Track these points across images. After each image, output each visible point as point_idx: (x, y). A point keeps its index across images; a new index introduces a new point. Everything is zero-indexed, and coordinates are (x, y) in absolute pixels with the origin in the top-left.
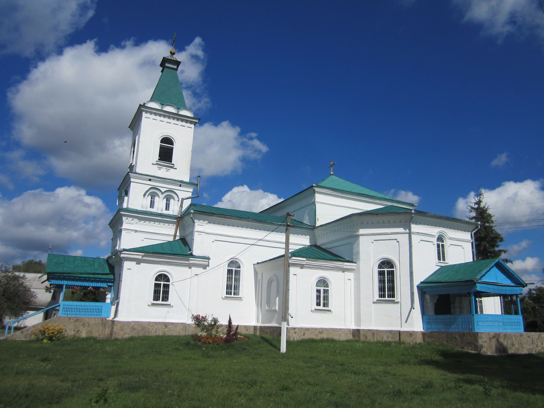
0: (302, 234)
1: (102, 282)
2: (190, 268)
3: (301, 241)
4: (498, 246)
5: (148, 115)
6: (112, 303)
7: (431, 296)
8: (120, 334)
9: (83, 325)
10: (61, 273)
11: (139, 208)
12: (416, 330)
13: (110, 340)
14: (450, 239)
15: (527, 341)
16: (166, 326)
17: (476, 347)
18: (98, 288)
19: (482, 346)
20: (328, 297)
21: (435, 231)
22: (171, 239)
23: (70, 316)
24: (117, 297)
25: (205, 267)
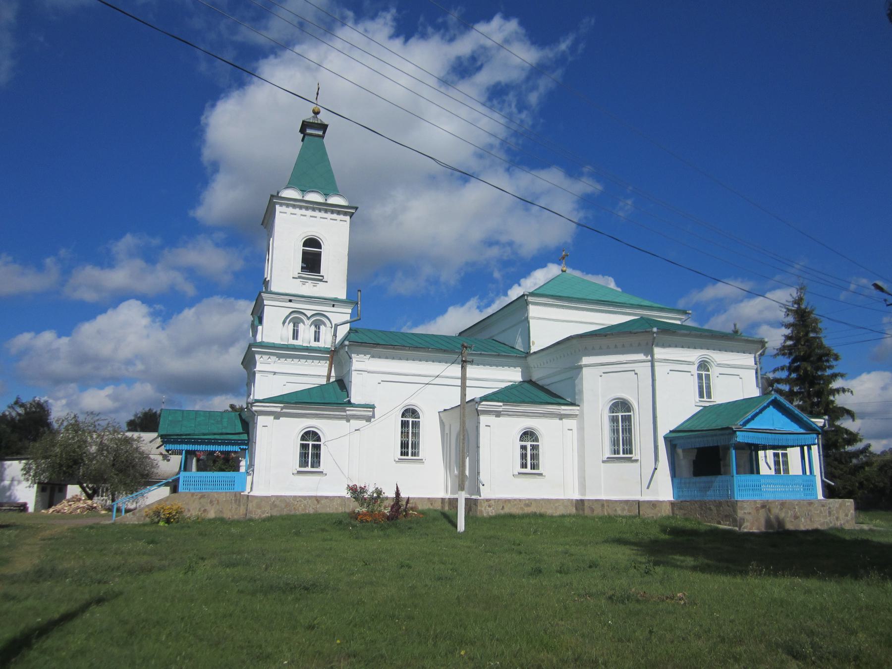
0: (503, 365)
1: (233, 444)
2: (348, 421)
3: (513, 375)
4: (830, 367)
5: (284, 209)
6: (247, 473)
7: (684, 451)
8: (258, 514)
9: (211, 502)
10: (178, 435)
11: (278, 341)
12: (661, 499)
13: (247, 522)
14: (719, 365)
15: (821, 512)
16: (318, 501)
17: (735, 522)
18: (229, 453)
19: (743, 520)
20: (537, 455)
21: (694, 355)
24: (251, 465)
25: (368, 419)
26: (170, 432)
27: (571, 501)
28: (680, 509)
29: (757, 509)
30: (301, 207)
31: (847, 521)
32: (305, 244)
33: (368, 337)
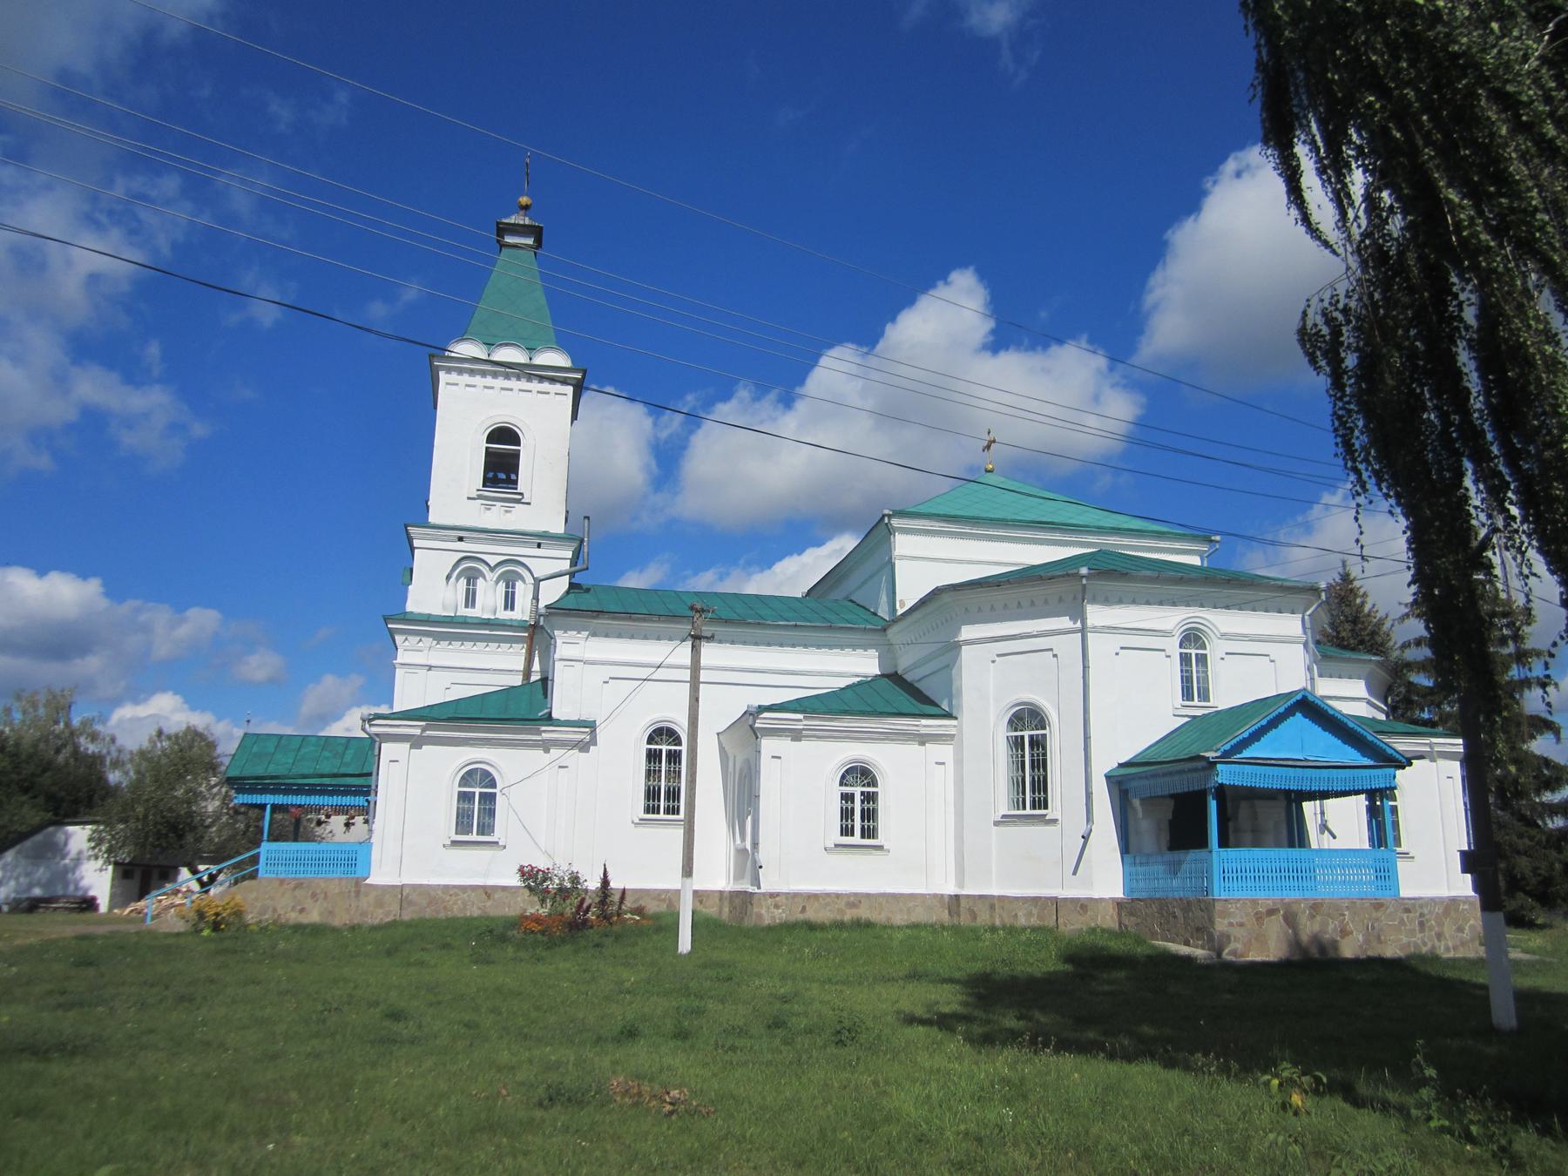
0: (854, 647)
2: (547, 751)
3: (863, 664)
5: (454, 377)
7: (1143, 800)
9: (314, 895)
11: (436, 610)
14: (1225, 636)
15: (1402, 922)
19: (1227, 938)
21: (1172, 619)
22: (517, 680)
23: (283, 876)
25: (583, 747)
26: (246, 773)
27: (939, 897)
28: (1131, 914)
29: (1259, 917)
30: (484, 374)
31: (1463, 944)
32: (490, 439)
33: (590, 604)
